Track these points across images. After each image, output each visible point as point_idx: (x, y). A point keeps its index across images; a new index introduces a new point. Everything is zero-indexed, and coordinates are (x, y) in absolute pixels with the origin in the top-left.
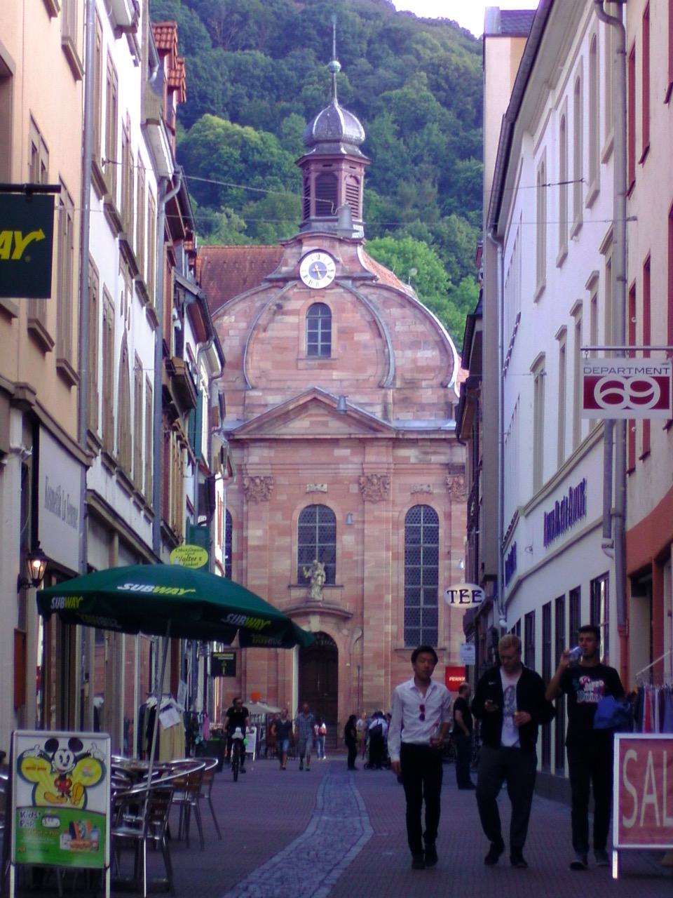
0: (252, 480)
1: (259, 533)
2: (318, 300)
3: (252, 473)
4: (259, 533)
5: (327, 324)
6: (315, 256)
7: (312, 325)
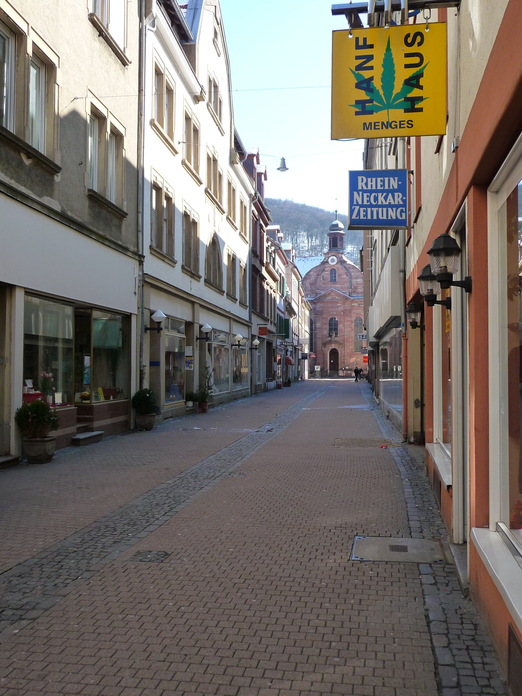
0: (318, 311)
1: (319, 324)
2: (333, 267)
3: (317, 310)
4: (319, 324)
5: (335, 274)
6: (332, 257)
7: (331, 274)
